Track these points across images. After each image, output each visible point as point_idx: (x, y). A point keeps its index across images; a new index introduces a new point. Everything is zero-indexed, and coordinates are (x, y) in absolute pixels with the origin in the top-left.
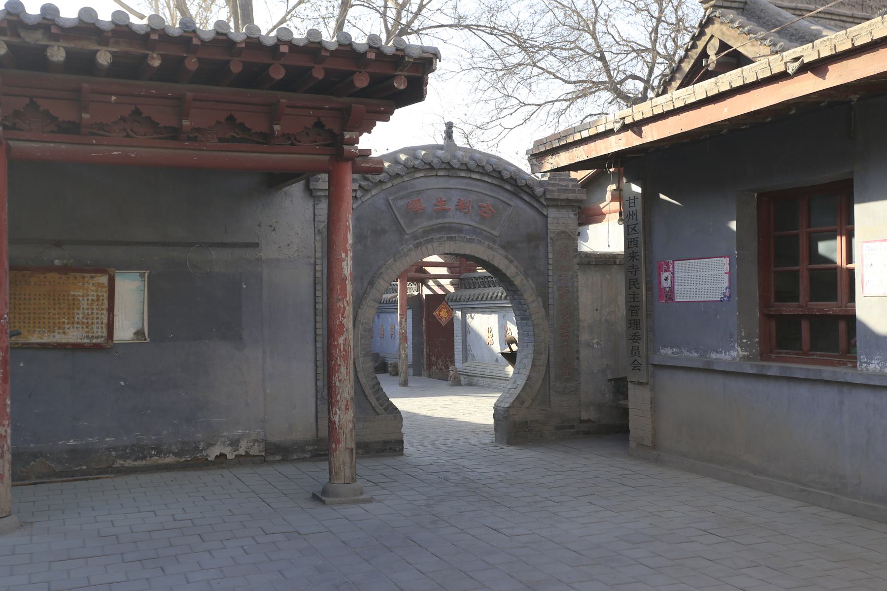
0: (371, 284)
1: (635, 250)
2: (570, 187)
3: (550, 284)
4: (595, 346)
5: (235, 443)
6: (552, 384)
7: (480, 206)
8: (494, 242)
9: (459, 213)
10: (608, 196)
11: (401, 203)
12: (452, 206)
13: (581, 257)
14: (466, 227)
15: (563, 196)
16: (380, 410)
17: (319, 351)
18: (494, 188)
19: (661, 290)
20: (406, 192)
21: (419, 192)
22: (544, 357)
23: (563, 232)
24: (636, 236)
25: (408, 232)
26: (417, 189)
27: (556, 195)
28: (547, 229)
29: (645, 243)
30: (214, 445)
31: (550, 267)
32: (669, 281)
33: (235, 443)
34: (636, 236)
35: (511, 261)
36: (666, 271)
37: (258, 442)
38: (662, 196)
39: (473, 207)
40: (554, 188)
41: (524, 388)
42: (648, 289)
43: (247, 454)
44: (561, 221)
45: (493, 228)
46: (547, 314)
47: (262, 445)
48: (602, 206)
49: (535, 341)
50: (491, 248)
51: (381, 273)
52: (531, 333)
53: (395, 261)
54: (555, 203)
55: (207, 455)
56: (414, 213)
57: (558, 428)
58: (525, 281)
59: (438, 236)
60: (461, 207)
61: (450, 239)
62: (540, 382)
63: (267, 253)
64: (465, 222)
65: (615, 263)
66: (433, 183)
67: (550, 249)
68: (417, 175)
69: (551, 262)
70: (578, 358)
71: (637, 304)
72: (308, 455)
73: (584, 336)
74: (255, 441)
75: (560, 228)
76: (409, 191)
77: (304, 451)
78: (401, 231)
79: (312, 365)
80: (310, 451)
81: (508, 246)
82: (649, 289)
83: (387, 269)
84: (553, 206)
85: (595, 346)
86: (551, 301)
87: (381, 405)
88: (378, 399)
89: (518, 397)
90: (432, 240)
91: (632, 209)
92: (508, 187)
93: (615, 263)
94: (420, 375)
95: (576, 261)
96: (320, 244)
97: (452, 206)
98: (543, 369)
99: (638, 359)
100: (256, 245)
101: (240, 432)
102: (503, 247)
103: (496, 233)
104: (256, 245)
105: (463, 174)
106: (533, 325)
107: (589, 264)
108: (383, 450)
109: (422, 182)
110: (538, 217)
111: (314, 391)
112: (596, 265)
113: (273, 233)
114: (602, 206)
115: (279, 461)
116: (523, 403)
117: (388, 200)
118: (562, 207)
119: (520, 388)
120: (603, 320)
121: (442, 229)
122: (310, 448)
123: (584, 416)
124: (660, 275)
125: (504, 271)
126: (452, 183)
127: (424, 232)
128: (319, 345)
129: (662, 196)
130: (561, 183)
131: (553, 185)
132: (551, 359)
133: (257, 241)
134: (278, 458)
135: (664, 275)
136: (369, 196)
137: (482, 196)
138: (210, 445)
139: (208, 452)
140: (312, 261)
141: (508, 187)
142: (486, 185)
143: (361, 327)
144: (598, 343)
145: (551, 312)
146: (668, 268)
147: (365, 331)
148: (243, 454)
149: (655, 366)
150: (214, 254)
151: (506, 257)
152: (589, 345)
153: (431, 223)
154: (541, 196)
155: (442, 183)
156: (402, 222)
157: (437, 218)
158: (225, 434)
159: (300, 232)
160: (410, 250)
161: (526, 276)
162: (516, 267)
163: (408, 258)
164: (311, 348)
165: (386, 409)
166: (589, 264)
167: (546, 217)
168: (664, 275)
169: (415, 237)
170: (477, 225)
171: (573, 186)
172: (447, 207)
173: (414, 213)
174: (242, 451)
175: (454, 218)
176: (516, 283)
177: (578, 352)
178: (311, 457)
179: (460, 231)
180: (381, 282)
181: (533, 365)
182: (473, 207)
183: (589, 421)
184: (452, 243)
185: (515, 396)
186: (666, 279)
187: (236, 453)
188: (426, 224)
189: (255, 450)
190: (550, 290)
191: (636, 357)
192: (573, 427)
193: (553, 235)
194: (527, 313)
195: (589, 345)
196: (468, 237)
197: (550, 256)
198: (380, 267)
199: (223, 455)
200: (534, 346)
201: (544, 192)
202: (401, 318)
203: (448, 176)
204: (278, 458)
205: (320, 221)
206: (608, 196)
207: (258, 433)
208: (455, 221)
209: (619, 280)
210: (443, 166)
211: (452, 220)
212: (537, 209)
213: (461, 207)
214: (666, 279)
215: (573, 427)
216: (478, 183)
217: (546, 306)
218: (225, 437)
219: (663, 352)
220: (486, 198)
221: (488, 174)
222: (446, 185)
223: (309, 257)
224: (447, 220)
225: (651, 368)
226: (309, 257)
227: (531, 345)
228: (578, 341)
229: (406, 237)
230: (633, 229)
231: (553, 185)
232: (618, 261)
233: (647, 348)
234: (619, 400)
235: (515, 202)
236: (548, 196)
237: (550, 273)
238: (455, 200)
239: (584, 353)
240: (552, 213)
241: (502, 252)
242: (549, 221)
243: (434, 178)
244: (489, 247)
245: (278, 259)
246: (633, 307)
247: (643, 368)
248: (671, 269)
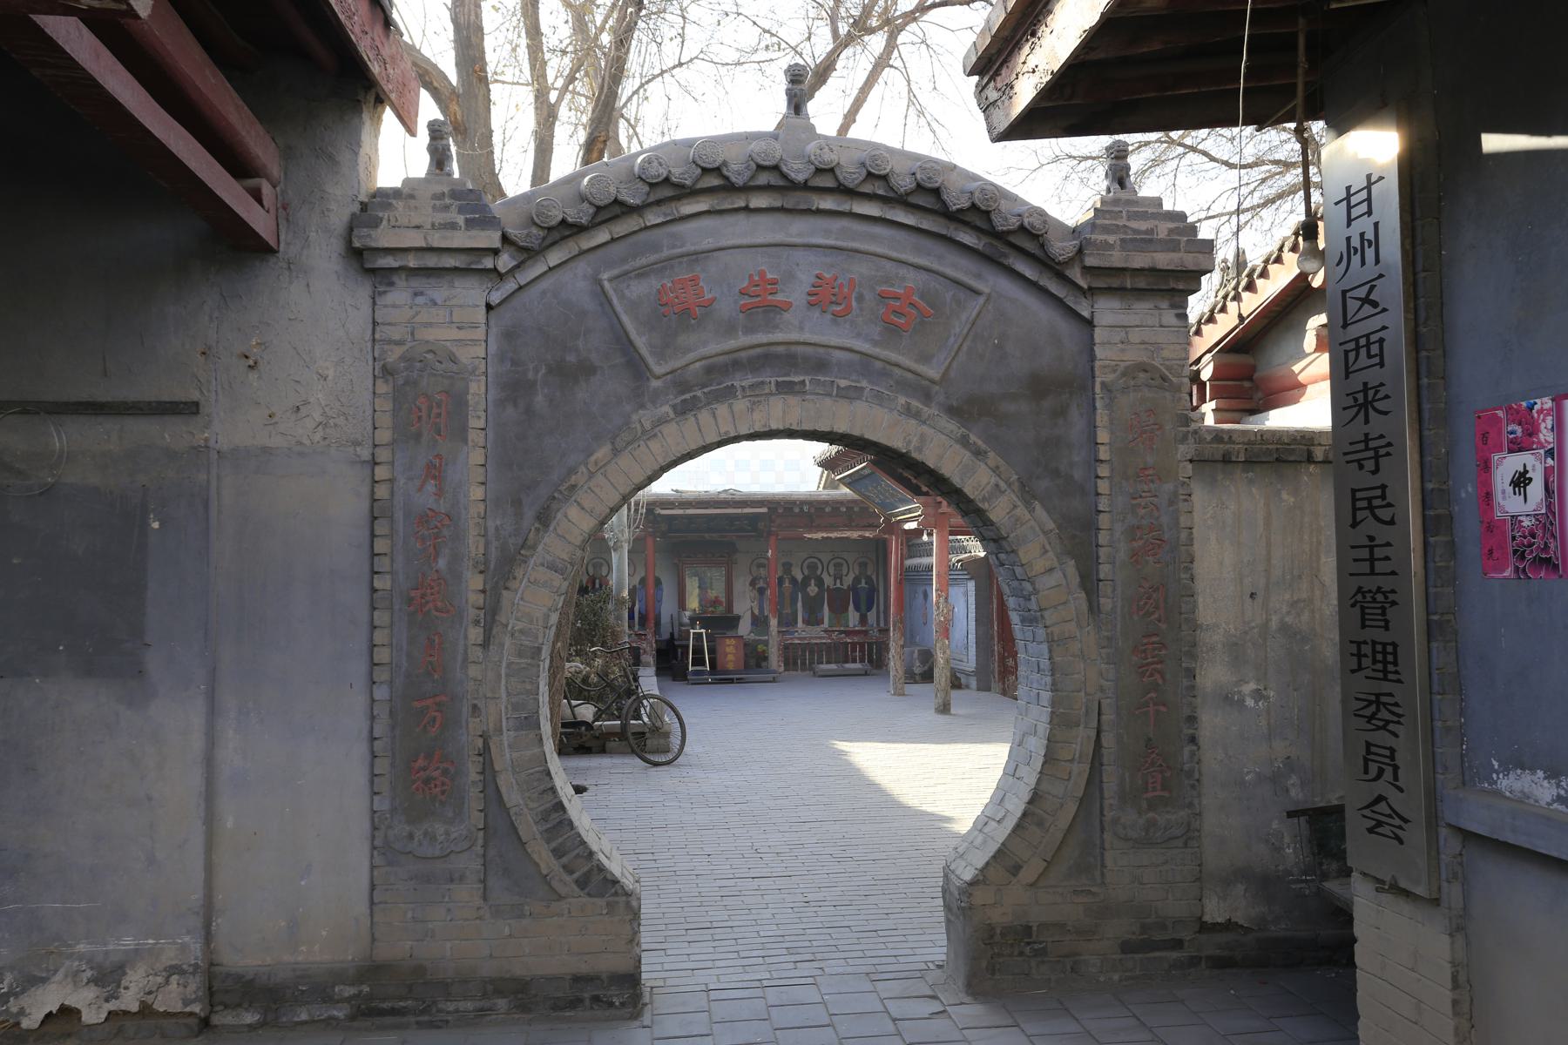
0: (544, 518)
1: (1373, 376)
2: (1162, 234)
3: (1104, 520)
4: (1250, 702)
5: (108, 977)
6: (1109, 815)
7: (883, 296)
8: (927, 397)
9: (816, 313)
10: (1310, 341)
11: (639, 289)
12: (796, 295)
13: (1201, 441)
14: (838, 354)
15: (1139, 261)
16: (565, 883)
17: (382, 712)
18: (927, 243)
19: (1491, 527)
20: (653, 258)
21: (696, 256)
22: (1082, 738)
23: (1143, 368)
24: (1376, 323)
25: (658, 370)
26: (689, 248)
27: (1116, 259)
28: (1092, 358)
29: (1416, 341)
30: (44, 980)
31: (1103, 471)
32: (1536, 490)
33: (108, 977)
34: (1376, 323)
35: (978, 453)
36: (1517, 447)
37: (182, 972)
38: (1493, 142)
39: (860, 298)
40: (1111, 239)
41: (1018, 827)
42: (1430, 526)
43: (146, 1011)
44: (1135, 336)
45: (925, 358)
46: (1094, 608)
47: (194, 985)
48: (1296, 368)
49: (1055, 688)
50: (916, 415)
51: (573, 487)
52: (1045, 664)
53: (616, 452)
54: (1115, 283)
55: (22, 1012)
56: (679, 316)
57: (1127, 947)
58: (1021, 511)
59: (750, 380)
60: (823, 298)
61: (786, 388)
62: (1072, 808)
63: (230, 427)
64: (834, 341)
65: (1310, 459)
66: (737, 230)
67: (1102, 416)
68: (688, 208)
69: (1104, 453)
70: (1193, 740)
71: (1387, 583)
72: (339, 1013)
73: (1214, 674)
74: (172, 970)
75: (1133, 356)
76: (666, 253)
77: (329, 1000)
78: (636, 367)
79: (361, 750)
80: (348, 1000)
81: (969, 410)
82: (1436, 523)
83: (591, 475)
84: (1110, 291)
85: (1250, 702)
86: (1105, 570)
87: (568, 869)
88: (558, 853)
89: (999, 855)
90: (730, 393)
91: (1365, 225)
92: (968, 238)
93: (1310, 459)
94: (988, 689)
95: (1185, 450)
96: (388, 406)
97: (796, 295)
98: (1081, 771)
99: (1391, 793)
100: (191, 409)
101: (128, 942)
102: (953, 411)
103: (933, 372)
104: (191, 409)
105: (828, 203)
106: (1051, 641)
107: (1226, 460)
108: (575, 1003)
109: (703, 231)
110: (1064, 326)
111: (367, 825)
112: (1250, 463)
113: (253, 376)
114: (1296, 368)
115: (251, 1027)
116: (1015, 869)
117: (599, 283)
118: (1140, 293)
119: (1010, 824)
120: (1274, 624)
121: (764, 359)
122: (349, 991)
123: (1215, 911)
124: (1486, 467)
125: (956, 481)
126: (797, 229)
127: (709, 370)
128: (381, 693)
129: (1493, 142)
130: (1134, 224)
131: (1107, 230)
132: (1108, 740)
133: (195, 395)
134: (250, 1018)
135: (1507, 466)
136: (540, 268)
137: (889, 265)
138: (33, 981)
139: (25, 1001)
140: (365, 454)
141: (968, 238)
142: (901, 235)
143: (508, 641)
144: (1258, 695)
145: (1106, 603)
146: (1532, 431)
147: (520, 655)
148: (134, 1007)
149: (1468, 836)
150: (62, 436)
151: (964, 442)
152: (1229, 700)
153: (732, 344)
154: (1069, 262)
155: (765, 230)
156: (641, 342)
157: (749, 330)
158: (82, 947)
159: (331, 373)
160: (662, 421)
161: (1027, 493)
162: (996, 470)
163: (654, 445)
164: (359, 701)
165: (582, 883)
166: (1226, 460)
167: (1089, 323)
168: (1507, 466)
169: (683, 386)
170: (877, 351)
171: (1171, 231)
172: (780, 297)
173: (679, 316)
174: (129, 1001)
175: (803, 328)
176: (993, 517)
177: (1192, 719)
178: (352, 1018)
179: (821, 366)
180: (573, 512)
181: (1050, 759)
182: (860, 298)
183: (1229, 926)
184: (793, 400)
185: (993, 848)
186: (1521, 481)
187: (112, 1006)
188: (714, 346)
189: (170, 999)
190: (1103, 538)
191: (1382, 787)
192: (1178, 944)
193: (1109, 378)
194: (1033, 605)
195: (1229, 700)
196: (843, 383)
197: (1103, 436)
198: (572, 471)
199: (67, 1013)
200: (1053, 704)
201: (1080, 251)
202: (939, 596)
203: (782, 210)
204: (250, 1018)
205: (390, 342)
206: (1310, 341)
207: (184, 948)
208: (806, 336)
209: (1317, 502)
210: (763, 179)
211: (794, 336)
212: (1059, 302)
213: (823, 298)
214: (1521, 481)
215: (1178, 944)
216: (878, 230)
217: (1089, 583)
218: (81, 957)
219: (1511, 783)
220: (903, 271)
221: (901, 201)
222: (779, 237)
223: (356, 443)
224: (779, 336)
225: (1450, 845)
226: (356, 443)
227: (1046, 696)
228: (1193, 687)
229: (655, 383)
230: (1366, 300)
231: (1107, 230)
232: (1319, 454)
233: (1432, 759)
234: (1325, 876)
235: (992, 283)
236: (1090, 261)
237: (1103, 487)
238: (805, 279)
239: (1211, 722)
240: (1107, 312)
241: (952, 426)
242: (1099, 334)
243: (741, 218)
244: (908, 412)
245: (265, 450)
246: (1368, 601)
247: (1416, 835)
248: (1546, 435)
